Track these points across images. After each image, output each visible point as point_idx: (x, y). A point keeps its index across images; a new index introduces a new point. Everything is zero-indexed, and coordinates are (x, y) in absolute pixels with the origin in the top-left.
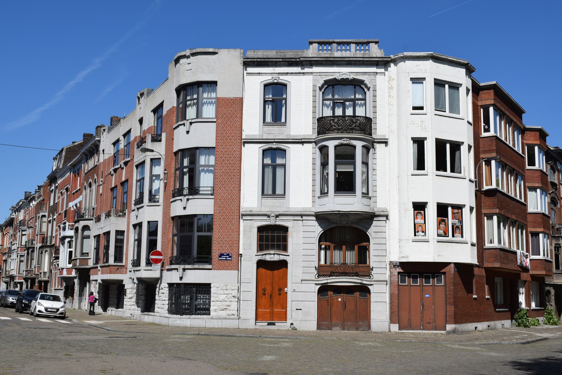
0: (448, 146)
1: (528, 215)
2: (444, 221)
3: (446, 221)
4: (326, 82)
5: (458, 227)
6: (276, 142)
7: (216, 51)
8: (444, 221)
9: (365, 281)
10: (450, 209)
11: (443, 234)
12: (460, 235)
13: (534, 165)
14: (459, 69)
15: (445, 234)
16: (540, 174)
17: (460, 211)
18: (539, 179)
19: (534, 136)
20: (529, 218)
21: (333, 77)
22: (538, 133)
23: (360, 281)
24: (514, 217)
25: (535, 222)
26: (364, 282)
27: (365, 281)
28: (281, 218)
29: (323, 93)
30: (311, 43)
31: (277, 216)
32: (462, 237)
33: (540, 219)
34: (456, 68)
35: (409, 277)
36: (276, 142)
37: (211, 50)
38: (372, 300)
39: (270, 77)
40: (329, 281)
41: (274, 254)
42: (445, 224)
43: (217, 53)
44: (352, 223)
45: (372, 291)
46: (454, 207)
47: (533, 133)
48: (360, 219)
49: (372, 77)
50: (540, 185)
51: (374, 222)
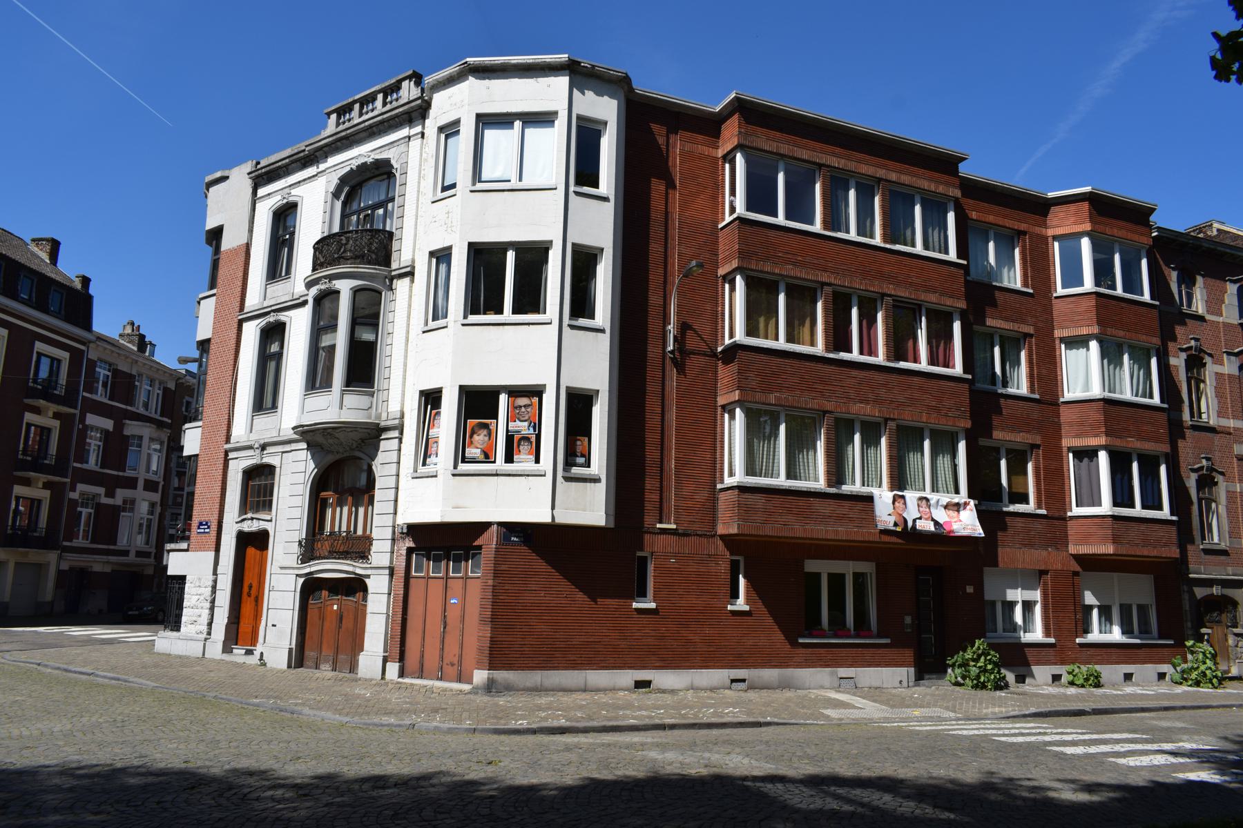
0: (511, 256)
1: (1062, 409)
2: (486, 426)
3: (493, 427)
4: (343, 180)
5: (526, 439)
6: (274, 311)
7: (226, 173)
8: (486, 426)
9: (358, 568)
10: (503, 398)
11: (482, 457)
12: (533, 458)
13: (1080, 283)
14: (552, 78)
15: (487, 456)
16: (1093, 303)
17: (536, 400)
18: (1093, 315)
19: (1076, 214)
20: (1066, 415)
21: (348, 169)
22: (1086, 205)
23: (350, 569)
24: (868, 411)
25: (1081, 424)
26: (359, 571)
27: (358, 568)
28: (270, 450)
29: (345, 204)
30: (329, 114)
31: (263, 447)
32: (537, 461)
33: (1096, 415)
34: (540, 80)
35: (429, 559)
36: (274, 311)
37: (218, 175)
38: (369, 609)
39: (279, 197)
40: (313, 569)
41: (252, 519)
42: (490, 434)
43: (227, 178)
44: (352, 449)
45: (370, 590)
46: (515, 392)
47: (1072, 208)
48: (363, 440)
49: (403, 148)
50: (1095, 330)
51: (382, 443)
